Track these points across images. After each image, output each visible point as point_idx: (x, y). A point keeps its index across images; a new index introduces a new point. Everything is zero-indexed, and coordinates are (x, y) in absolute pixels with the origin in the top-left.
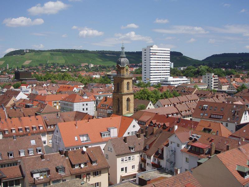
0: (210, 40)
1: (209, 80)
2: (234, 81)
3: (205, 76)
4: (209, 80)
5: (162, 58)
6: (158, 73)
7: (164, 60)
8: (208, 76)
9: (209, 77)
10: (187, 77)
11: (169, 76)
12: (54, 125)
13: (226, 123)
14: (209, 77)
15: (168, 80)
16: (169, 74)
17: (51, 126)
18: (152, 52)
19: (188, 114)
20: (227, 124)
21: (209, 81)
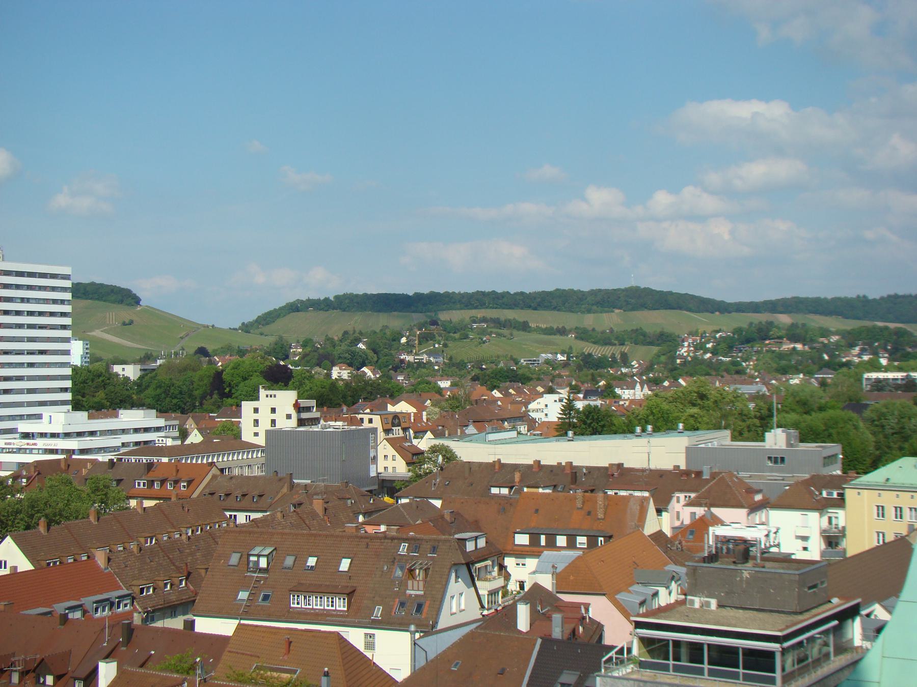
2: (393, 425)
5: (31, 313)
7: (55, 302)
8: (272, 403)
9: (273, 410)
10: (162, 411)
11: (70, 407)
13: (366, 634)
14: (273, 410)
16: (68, 296)
19: (173, 598)
20: (372, 636)
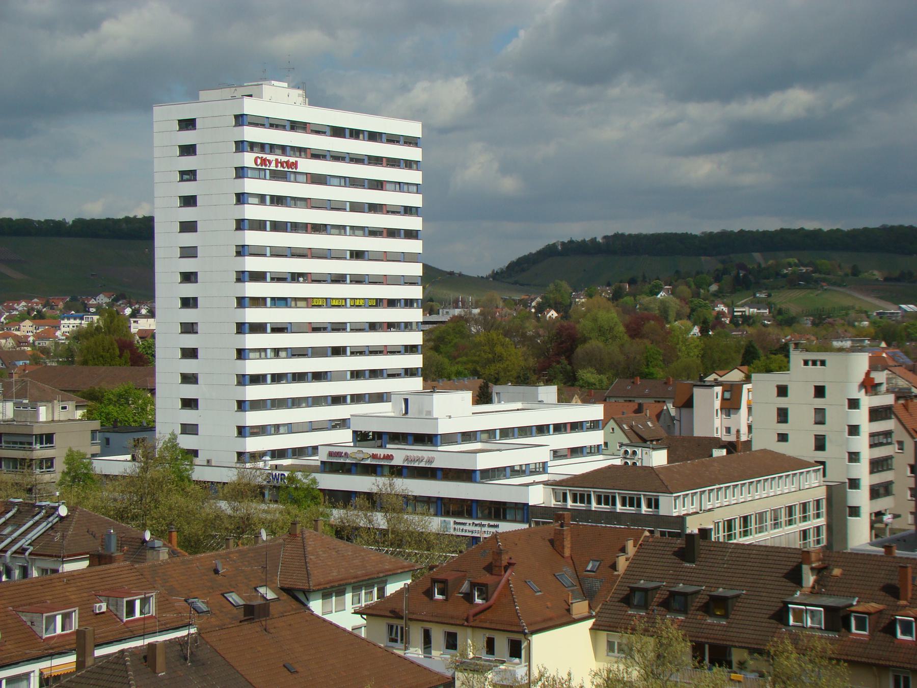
0: (652, 322)
1: (820, 417)
3: (779, 378)
4: (820, 417)
6: (393, 375)
8: (817, 375)
9: (820, 392)
12: (657, 440)
15: (443, 428)
17: (652, 441)
18: (253, 146)
21: (820, 430)
